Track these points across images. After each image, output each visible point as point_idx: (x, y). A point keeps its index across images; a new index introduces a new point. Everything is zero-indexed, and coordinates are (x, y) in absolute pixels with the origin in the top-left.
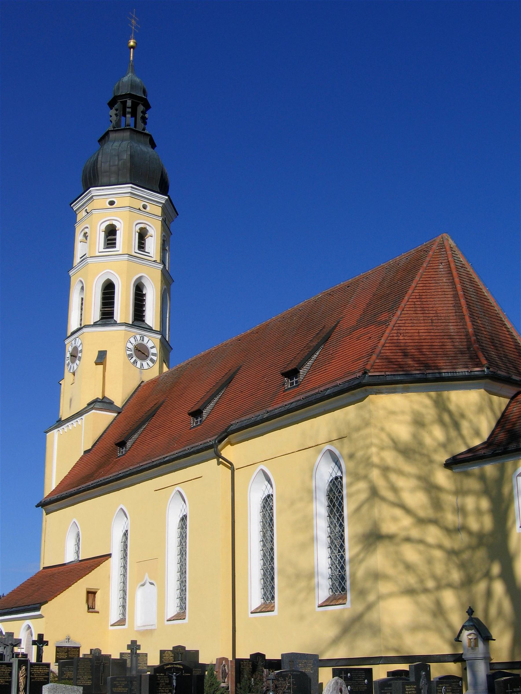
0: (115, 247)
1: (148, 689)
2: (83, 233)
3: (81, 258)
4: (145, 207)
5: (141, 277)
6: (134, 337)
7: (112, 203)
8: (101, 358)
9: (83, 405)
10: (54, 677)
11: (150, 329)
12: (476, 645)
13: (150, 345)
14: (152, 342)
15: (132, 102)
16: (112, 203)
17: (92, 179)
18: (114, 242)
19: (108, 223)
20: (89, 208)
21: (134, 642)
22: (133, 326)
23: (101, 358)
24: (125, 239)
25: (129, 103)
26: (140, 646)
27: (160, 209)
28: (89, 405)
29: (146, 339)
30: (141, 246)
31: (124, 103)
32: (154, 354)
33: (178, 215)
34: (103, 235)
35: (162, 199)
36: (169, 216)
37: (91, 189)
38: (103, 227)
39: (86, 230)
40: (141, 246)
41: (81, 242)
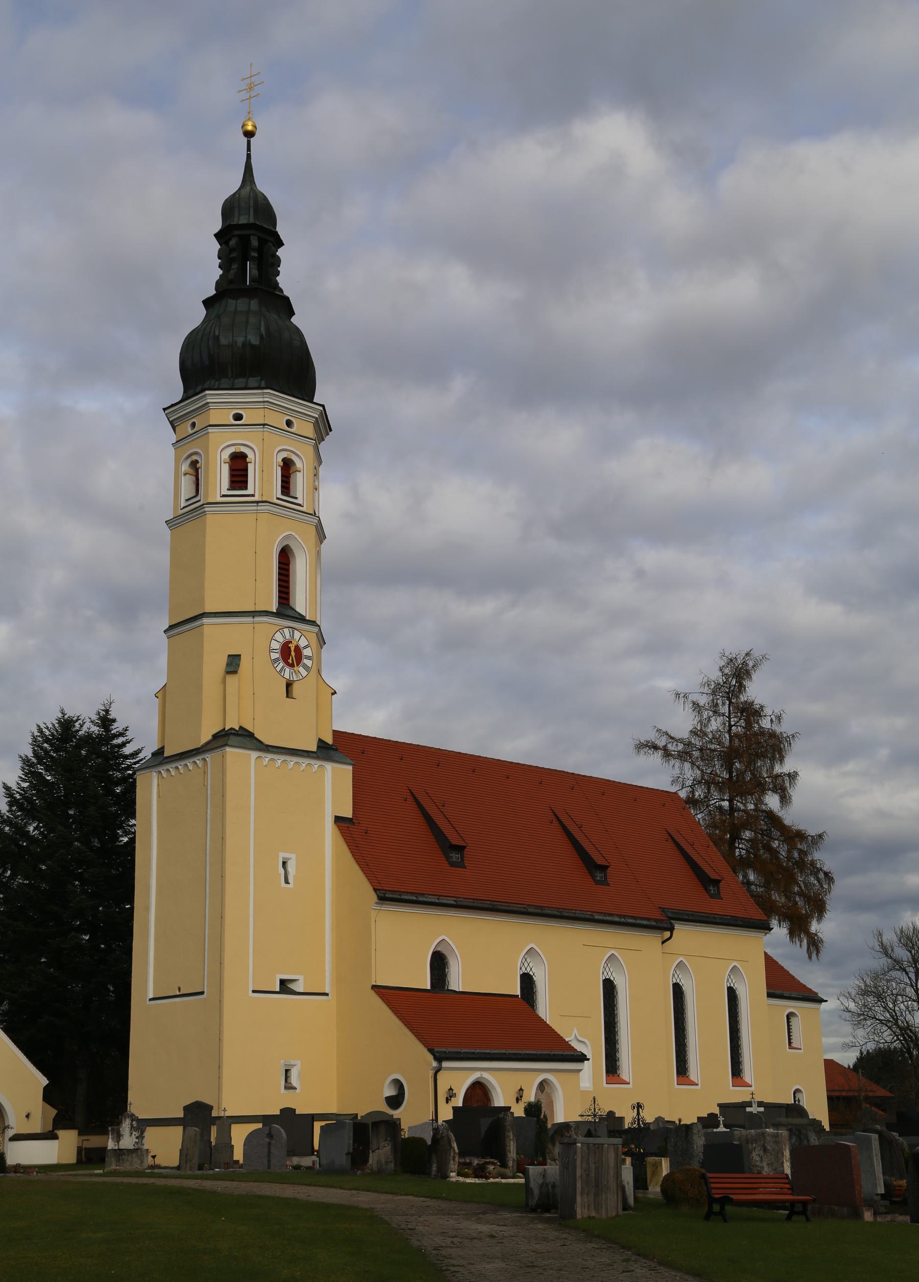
0: (246, 488)
2: (189, 462)
3: (187, 500)
4: (289, 423)
7: (238, 417)
8: (233, 664)
9: (206, 737)
10: (801, 852)
12: (753, 666)
13: (303, 643)
16: (238, 417)
18: (235, 473)
19: (232, 450)
20: (200, 422)
22: (278, 614)
23: (233, 664)
25: (255, 242)
28: (216, 737)
29: (297, 635)
30: (286, 487)
32: (308, 658)
33: (331, 430)
34: (226, 469)
37: (207, 392)
38: (226, 455)
39: (194, 458)
40: (286, 487)
41: (185, 474)
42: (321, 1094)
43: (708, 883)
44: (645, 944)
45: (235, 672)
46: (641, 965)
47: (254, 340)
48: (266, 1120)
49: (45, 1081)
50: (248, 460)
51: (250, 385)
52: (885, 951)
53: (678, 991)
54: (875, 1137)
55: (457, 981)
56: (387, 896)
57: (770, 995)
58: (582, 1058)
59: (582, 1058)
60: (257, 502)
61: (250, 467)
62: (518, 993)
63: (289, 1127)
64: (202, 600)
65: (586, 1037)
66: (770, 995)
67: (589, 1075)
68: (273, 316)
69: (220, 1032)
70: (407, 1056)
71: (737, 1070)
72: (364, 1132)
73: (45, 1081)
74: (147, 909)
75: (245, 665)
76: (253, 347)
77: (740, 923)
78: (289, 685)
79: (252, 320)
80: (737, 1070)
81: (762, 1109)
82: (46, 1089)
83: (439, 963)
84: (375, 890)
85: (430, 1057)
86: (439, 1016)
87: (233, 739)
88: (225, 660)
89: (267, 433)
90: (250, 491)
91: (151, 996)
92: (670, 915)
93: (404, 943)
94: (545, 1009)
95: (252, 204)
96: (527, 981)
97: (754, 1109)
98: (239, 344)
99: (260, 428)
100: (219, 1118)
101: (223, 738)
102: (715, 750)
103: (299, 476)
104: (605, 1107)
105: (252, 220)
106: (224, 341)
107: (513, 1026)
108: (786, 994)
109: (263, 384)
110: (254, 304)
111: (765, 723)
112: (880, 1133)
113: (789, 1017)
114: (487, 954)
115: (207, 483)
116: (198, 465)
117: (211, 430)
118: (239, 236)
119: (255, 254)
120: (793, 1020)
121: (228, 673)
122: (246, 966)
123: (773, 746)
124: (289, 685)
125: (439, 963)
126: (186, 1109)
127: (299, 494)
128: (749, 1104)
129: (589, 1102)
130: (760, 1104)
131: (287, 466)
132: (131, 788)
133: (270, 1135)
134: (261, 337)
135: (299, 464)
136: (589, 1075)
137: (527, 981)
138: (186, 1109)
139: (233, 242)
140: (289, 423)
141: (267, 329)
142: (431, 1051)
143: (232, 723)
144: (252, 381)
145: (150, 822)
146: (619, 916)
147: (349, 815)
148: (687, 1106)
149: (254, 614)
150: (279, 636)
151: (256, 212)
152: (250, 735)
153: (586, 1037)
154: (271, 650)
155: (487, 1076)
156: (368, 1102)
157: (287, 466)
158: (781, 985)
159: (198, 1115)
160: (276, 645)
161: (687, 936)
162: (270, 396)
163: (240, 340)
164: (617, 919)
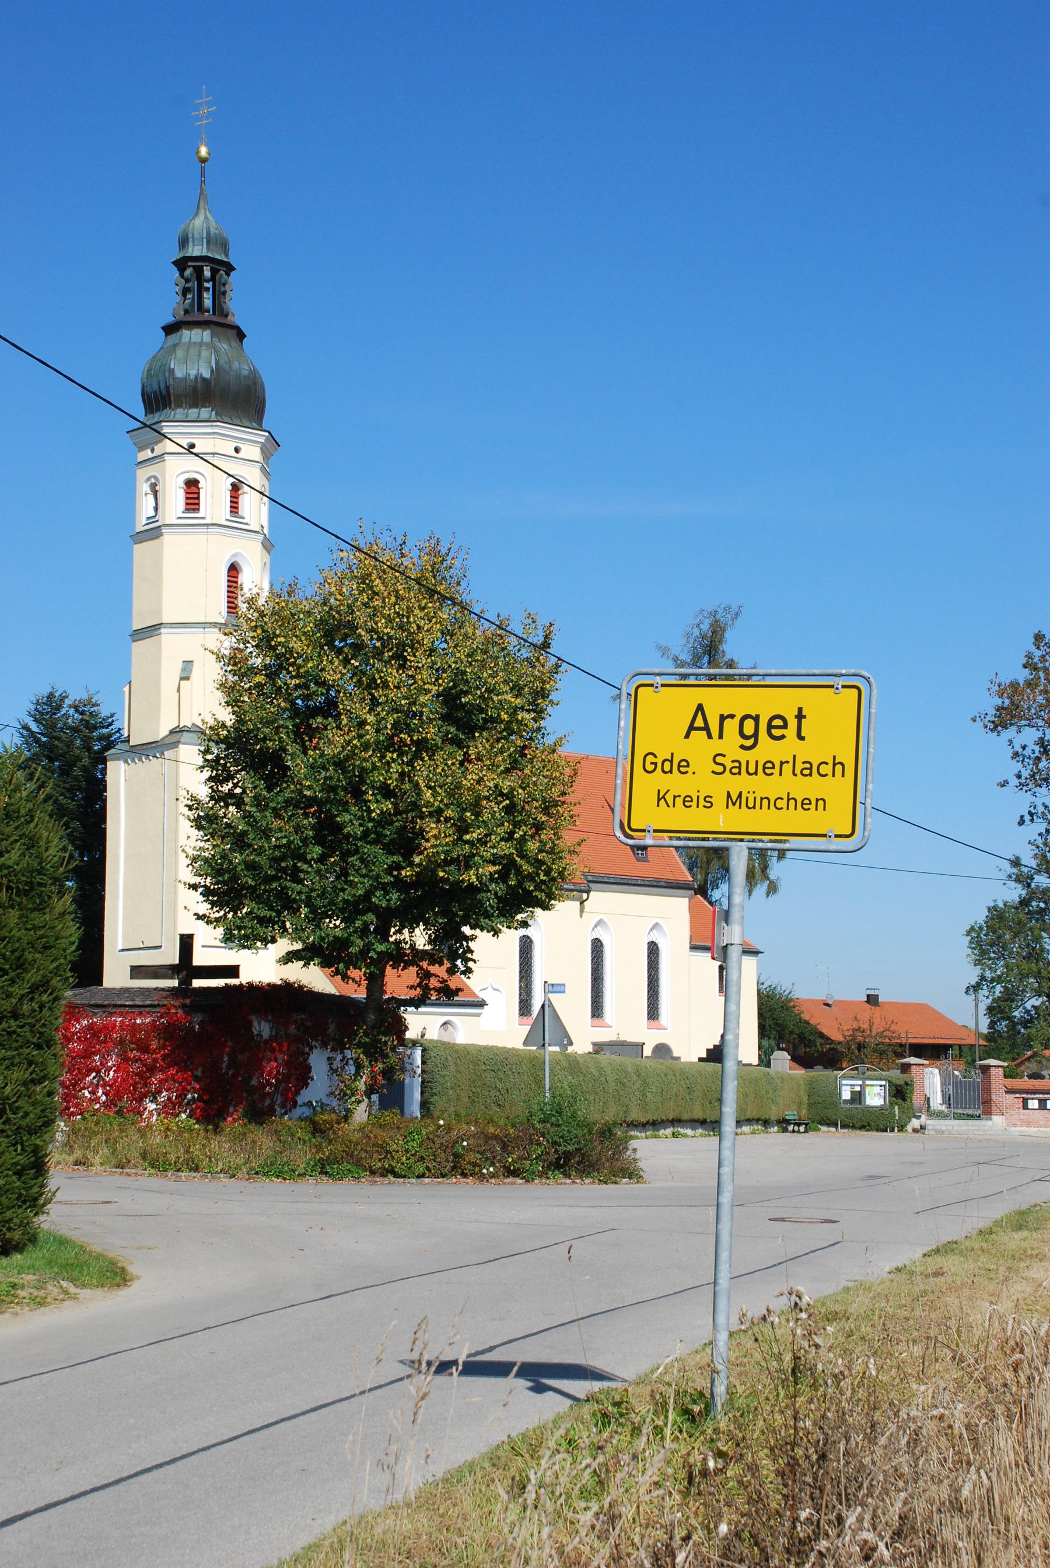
1: (134, 660)
5: (235, 555)
9: (163, 732)
15: (212, 269)
17: (161, 398)
25: (207, 273)
30: (234, 507)
31: (199, 271)
35: (261, 437)
36: (271, 446)
39: (153, 480)
40: (234, 507)
45: (187, 678)
47: (207, 374)
50: (200, 486)
52: (1024, 880)
57: (694, 948)
60: (207, 525)
61: (202, 492)
66: (694, 948)
68: (224, 346)
71: (653, 1012)
74: (117, 871)
75: (195, 674)
76: (204, 380)
77: (663, 884)
79: (205, 353)
80: (653, 1012)
88: (180, 665)
90: (201, 514)
91: (120, 948)
92: (590, 878)
95: (205, 235)
98: (192, 377)
102: (545, 1096)
105: (205, 253)
109: (213, 417)
110: (207, 335)
115: (164, 506)
116: (157, 488)
117: (167, 457)
119: (206, 285)
121: (182, 679)
134: (212, 371)
139: (188, 272)
140: (237, 450)
141: (217, 363)
143: (186, 722)
144: (205, 412)
145: (119, 804)
151: (208, 243)
163: (193, 373)
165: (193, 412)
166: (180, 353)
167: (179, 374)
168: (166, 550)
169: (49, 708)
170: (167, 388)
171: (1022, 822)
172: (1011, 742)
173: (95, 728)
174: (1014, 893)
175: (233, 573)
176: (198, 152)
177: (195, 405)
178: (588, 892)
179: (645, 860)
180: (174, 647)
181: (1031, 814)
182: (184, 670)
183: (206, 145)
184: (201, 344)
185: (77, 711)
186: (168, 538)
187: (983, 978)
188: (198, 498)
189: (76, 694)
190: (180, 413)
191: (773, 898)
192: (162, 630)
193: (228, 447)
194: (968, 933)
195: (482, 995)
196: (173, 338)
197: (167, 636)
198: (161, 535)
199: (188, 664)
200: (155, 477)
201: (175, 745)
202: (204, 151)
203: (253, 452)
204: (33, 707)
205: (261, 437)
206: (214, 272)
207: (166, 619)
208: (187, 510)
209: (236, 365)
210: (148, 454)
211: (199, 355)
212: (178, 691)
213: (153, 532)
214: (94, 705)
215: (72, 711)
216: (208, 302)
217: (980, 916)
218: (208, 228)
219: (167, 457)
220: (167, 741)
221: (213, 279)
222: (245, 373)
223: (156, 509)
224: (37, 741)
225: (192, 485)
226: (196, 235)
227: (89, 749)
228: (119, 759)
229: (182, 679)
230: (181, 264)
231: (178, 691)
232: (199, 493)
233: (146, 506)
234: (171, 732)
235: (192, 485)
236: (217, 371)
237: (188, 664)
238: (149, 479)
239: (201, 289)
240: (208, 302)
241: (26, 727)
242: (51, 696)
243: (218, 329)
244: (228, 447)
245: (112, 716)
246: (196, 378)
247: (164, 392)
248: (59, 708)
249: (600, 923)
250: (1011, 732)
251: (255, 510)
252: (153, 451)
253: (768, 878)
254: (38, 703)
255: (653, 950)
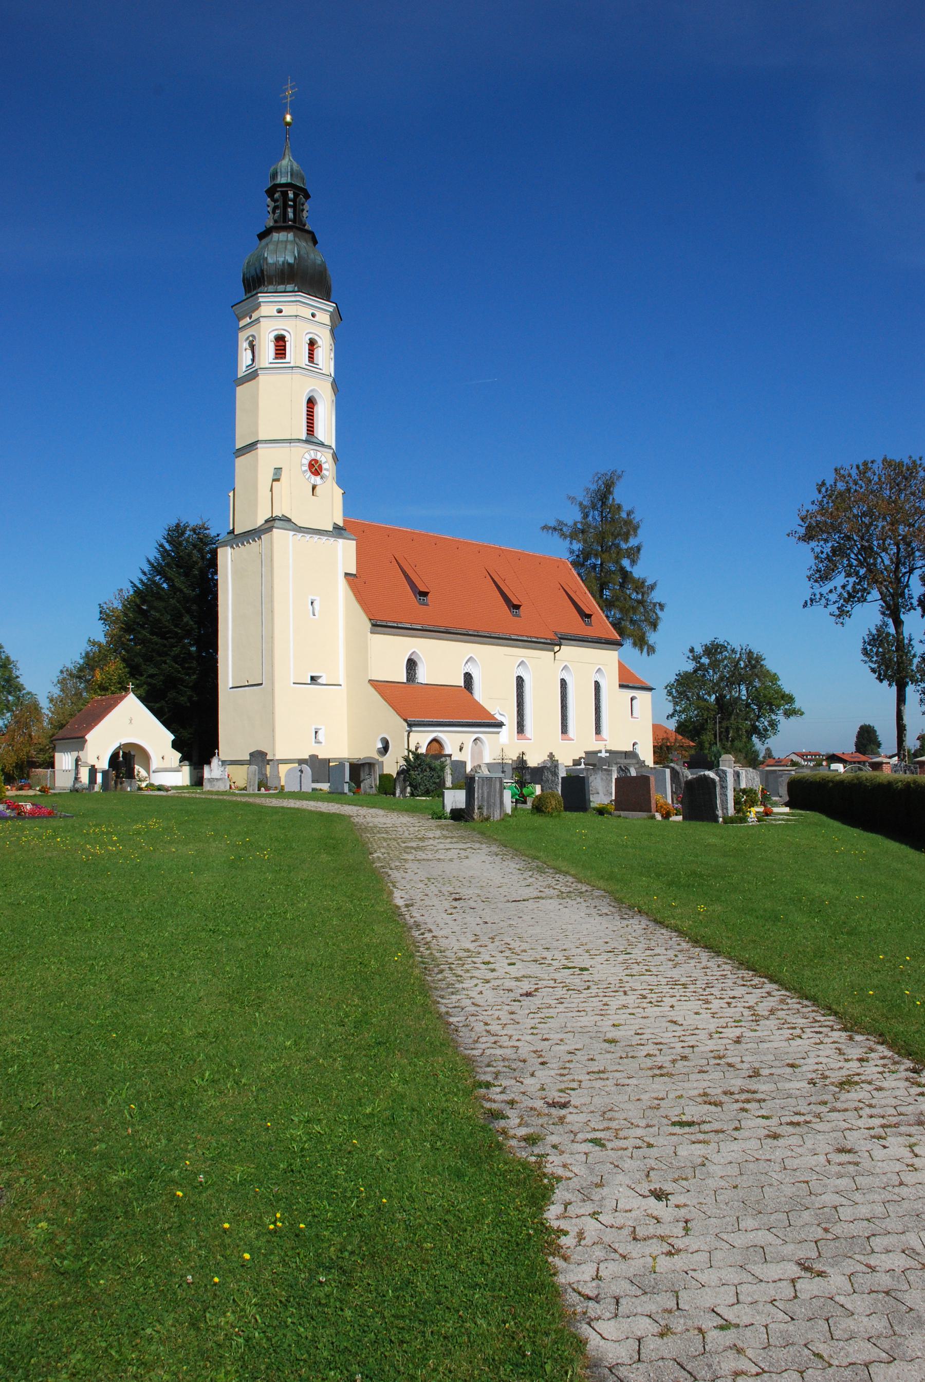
1: (237, 471)
4: (313, 315)
5: (311, 391)
6: (309, 453)
9: (260, 521)
11: (322, 444)
13: (323, 460)
14: (326, 459)
15: (294, 193)
16: (280, 311)
17: (256, 282)
19: (276, 333)
21: (802, 714)
22: (307, 441)
24: (296, 352)
25: (291, 195)
26: (881, 681)
27: (328, 317)
30: (311, 357)
31: (285, 194)
32: (326, 470)
35: (330, 307)
36: (338, 317)
38: (272, 336)
39: (251, 339)
40: (311, 357)
42: (339, 747)
43: (586, 616)
44: (545, 656)
45: (278, 480)
46: (541, 668)
47: (291, 260)
48: (301, 762)
49: (173, 737)
51: (288, 290)
52: (696, 659)
53: (563, 683)
54: (668, 771)
55: (424, 676)
56: (379, 626)
57: (621, 686)
58: (500, 725)
59: (500, 725)
61: (288, 344)
62: (462, 684)
63: (320, 767)
64: (257, 433)
65: (506, 712)
66: (621, 686)
67: (507, 733)
69: (273, 708)
70: (391, 724)
71: (598, 730)
72: (358, 770)
73: (173, 737)
75: (284, 476)
76: (289, 264)
78: (314, 488)
79: (289, 247)
80: (598, 730)
81: (608, 755)
82: (173, 741)
83: (411, 665)
84: (370, 620)
85: (406, 724)
86: (409, 698)
87: (277, 523)
89: (298, 322)
90: (287, 360)
91: (231, 686)
93: (389, 655)
94: (479, 694)
96: (468, 677)
97: (603, 755)
99: (294, 319)
100: (271, 760)
101: (271, 523)
103: (320, 350)
104: (567, 1160)
105: (289, 181)
106: (270, 261)
107: (460, 706)
108: (631, 685)
109: (296, 289)
110: (291, 236)
111: (624, 515)
112: (673, 769)
113: (632, 699)
114: (442, 661)
118: (281, 191)
120: (634, 702)
121: (274, 480)
122: (288, 668)
123: (629, 528)
124: (314, 488)
125: (411, 665)
126: (251, 755)
127: (320, 363)
128: (600, 751)
129: (499, 752)
130: (607, 751)
131: (312, 343)
132: (214, 553)
133: (301, 771)
135: (320, 342)
136: (507, 733)
137: (468, 677)
138: (251, 755)
139: (277, 195)
140: (313, 315)
142: (405, 720)
143: (278, 513)
144: (290, 287)
145: (227, 576)
146: (527, 637)
147: (354, 572)
148: (567, 755)
149: (290, 441)
150: (307, 456)
151: (292, 175)
152: (289, 520)
153: (506, 712)
154: (302, 465)
155: (440, 735)
156: (368, 751)
157: (312, 343)
158: (628, 682)
159: (259, 758)
160: (306, 462)
161: (568, 652)
162: (302, 297)
163: (281, 260)
164: (526, 639)
165: (281, 288)
166: (271, 247)
167: (270, 261)
168: (260, 386)
169: (176, 534)
170: (262, 271)
171: (805, 605)
172: (813, 549)
173: (206, 544)
174: (690, 667)
175: (310, 405)
176: (284, 118)
177: (282, 283)
178: (560, 645)
179: (590, 624)
180: (267, 458)
181: (811, 600)
182: (275, 474)
183: (291, 114)
184: (287, 241)
185: (195, 533)
186: (262, 378)
187: (675, 711)
188: (285, 350)
189: (194, 522)
190: (271, 288)
191: (652, 657)
192: (259, 445)
193: (307, 312)
194: (666, 688)
195: (500, 718)
196: (264, 242)
197: (262, 449)
198: (258, 375)
199: (278, 470)
200: (253, 336)
201: (270, 529)
202: (288, 118)
203: (324, 318)
204: (166, 533)
205: (330, 307)
206: (296, 195)
207: (261, 437)
208: (276, 358)
209: (312, 256)
210: (248, 320)
211: (286, 248)
212: (271, 490)
213: (253, 375)
214: (206, 529)
215: (192, 533)
216: (291, 215)
217: (672, 679)
218: (292, 166)
219: (261, 319)
220: (263, 528)
221: (294, 200)
222: (319, 262)
223: (253, 360)
224: (169, 555)
225: (280, 340)
226: (283, 170)
227: (203, 558)
228: (226, 546)
229: (274, 480)
230: (271, 192)
231: (271, 490)
232: (285, 346)
233: (245, 358)
234: (267, 521)
235: (280, 340)
236: (299, 259)
237: (278, 470)
238: (248, 338)
239: (285, 206)
240: (291, 215)
241: (162, 546)
242: (178, 525)
243: (299, 233)
244: (307, 312)
245: (218, 535)
246: (283, 263)
247: (260, 275)
248: (183, 533)
249: (565, 667)
250: (813, 544)
251: (325, 357)
252: (250, 318)
253: (647, 643)
254: (169, 530)
255: (597, 686)
